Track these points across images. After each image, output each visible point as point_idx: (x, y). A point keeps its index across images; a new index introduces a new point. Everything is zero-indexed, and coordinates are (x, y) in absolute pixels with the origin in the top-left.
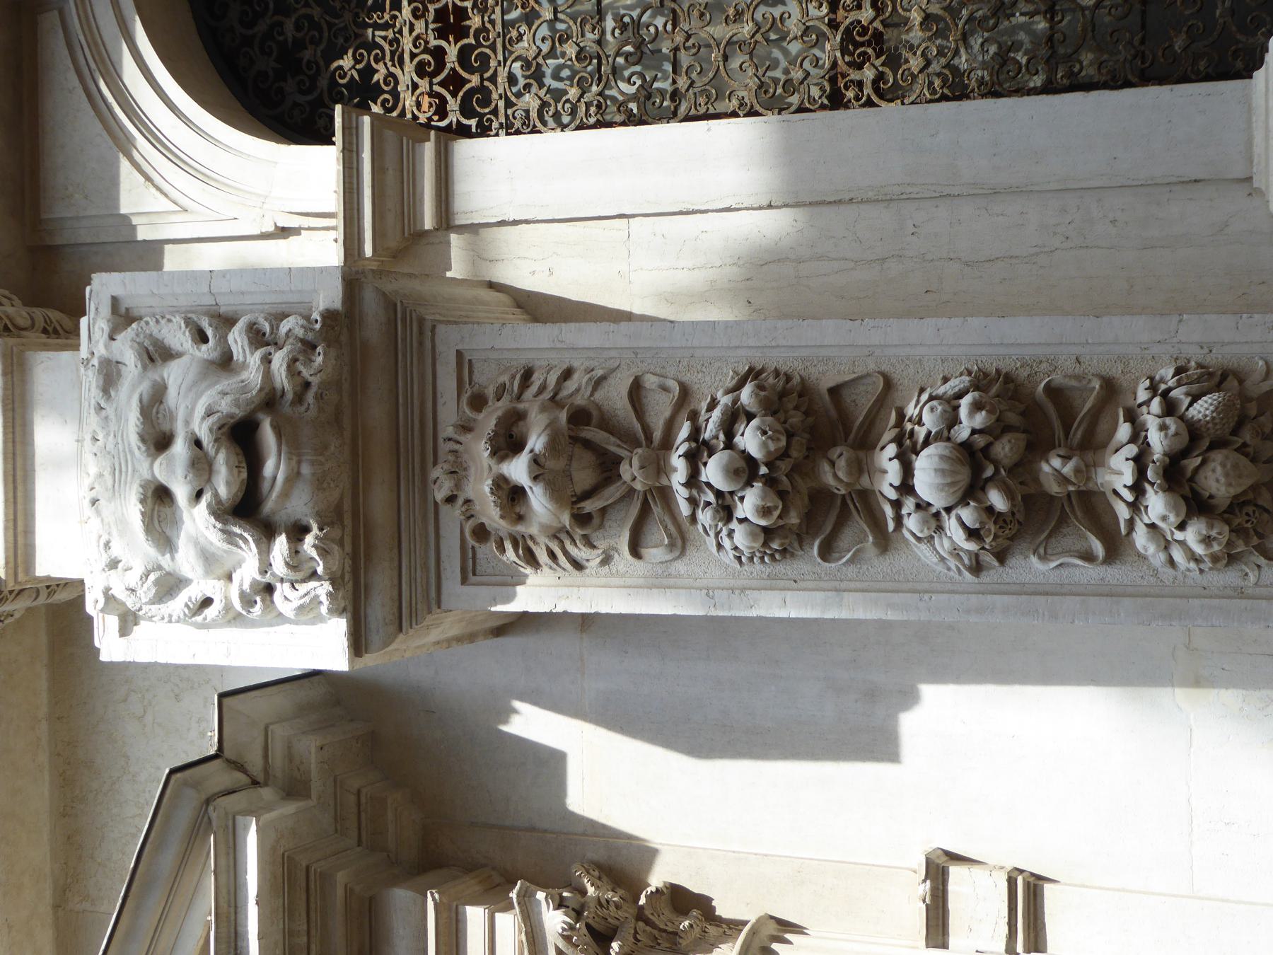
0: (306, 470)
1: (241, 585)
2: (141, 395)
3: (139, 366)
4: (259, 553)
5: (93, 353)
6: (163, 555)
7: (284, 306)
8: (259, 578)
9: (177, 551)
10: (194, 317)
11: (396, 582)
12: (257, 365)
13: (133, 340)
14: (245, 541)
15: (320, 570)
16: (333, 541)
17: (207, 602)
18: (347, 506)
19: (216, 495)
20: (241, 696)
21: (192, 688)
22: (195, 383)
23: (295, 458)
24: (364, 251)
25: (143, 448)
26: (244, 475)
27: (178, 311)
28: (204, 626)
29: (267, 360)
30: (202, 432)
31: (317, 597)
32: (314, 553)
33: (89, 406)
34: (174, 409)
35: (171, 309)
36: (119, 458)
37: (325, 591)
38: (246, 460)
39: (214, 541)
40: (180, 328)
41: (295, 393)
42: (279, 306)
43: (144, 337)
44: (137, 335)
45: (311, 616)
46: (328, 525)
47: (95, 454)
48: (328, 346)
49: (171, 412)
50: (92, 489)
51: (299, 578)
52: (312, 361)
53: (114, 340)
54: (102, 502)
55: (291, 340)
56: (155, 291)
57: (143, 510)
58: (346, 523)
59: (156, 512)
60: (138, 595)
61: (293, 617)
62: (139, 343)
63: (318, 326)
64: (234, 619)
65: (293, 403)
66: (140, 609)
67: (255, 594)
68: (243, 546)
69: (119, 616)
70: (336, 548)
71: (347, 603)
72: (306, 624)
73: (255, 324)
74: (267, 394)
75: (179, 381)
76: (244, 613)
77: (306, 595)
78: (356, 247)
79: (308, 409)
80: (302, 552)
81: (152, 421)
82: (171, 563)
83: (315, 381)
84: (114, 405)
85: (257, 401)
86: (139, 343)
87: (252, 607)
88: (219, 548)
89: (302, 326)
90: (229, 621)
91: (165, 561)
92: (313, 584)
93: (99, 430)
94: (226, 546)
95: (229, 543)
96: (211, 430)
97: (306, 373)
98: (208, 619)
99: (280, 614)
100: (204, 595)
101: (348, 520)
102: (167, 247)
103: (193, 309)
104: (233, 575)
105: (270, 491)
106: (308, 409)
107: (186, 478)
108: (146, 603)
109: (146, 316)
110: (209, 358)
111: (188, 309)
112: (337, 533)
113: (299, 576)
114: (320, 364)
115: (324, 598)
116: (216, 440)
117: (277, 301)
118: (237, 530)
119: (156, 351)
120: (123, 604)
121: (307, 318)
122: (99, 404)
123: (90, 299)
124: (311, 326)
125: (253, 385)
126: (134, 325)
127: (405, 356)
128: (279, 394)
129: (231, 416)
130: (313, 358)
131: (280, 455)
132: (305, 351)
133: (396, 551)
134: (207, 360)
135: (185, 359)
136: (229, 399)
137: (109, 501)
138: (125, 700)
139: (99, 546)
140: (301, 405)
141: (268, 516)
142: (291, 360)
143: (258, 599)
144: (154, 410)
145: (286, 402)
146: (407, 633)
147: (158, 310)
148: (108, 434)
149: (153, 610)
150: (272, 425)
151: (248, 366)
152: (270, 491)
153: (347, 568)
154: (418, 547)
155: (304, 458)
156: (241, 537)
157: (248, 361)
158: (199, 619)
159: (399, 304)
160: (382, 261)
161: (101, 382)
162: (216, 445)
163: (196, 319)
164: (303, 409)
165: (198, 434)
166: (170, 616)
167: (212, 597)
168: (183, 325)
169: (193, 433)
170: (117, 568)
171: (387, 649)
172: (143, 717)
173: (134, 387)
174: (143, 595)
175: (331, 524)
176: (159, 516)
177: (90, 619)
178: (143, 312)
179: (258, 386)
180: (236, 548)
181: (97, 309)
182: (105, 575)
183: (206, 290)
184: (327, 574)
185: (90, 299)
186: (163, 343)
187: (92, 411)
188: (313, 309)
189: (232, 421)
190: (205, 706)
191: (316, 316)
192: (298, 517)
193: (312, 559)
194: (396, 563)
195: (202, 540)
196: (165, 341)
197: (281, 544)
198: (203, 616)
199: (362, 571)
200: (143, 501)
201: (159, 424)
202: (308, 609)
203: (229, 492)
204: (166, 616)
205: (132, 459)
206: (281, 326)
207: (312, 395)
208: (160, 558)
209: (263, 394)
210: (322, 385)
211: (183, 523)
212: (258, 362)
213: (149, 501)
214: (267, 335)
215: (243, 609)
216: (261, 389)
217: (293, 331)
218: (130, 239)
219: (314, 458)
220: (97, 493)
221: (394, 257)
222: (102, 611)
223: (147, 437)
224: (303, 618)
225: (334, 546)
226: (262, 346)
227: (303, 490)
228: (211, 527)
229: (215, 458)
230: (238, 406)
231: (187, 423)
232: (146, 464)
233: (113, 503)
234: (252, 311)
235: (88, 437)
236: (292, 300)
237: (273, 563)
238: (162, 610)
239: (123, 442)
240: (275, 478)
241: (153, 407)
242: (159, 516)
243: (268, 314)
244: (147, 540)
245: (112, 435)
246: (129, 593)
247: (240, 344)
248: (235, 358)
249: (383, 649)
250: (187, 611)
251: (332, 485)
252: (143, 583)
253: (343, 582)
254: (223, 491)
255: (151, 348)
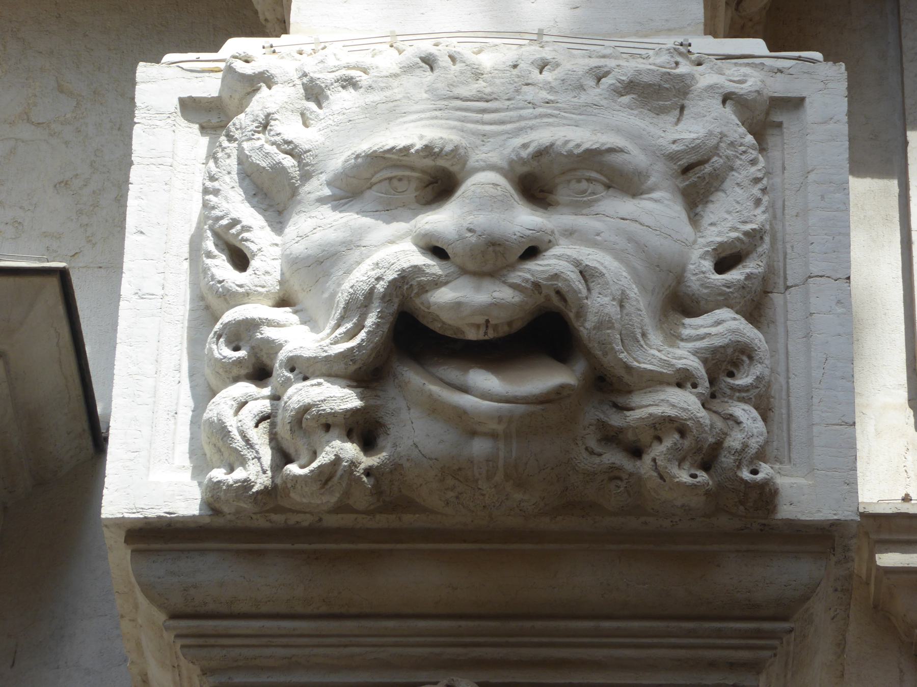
0: (480, 447)
1: (270, 323)
2: (621, 150)
3: (675, 147)
4: (328, 359)
5: (699, 64)
6: (329, 184)
7: (784, 411)
8: (282, 355)
9: (334, 208)
10: (765, 247)
11: (264, 609)
12: (674, 361)
13: (723, 136)
14: (351, 335)
15: (293, 469)
16: (347, 494)
17: (240, 260)
18: (409, 520)
19: (437, 283)
20: (61, 309)
21: (80, 212)
22: (641, 247)
23: (500, 428)
24: (887, 551)
25: (524, 154)
26: (472, 335)
27: (774, 217)
28: (196, 252)
29: (683, 380)
30: (552, 261)
31: (243, 462)
32: (324, 458)
33: (604, 57)
34: (597, 208)
35: (779, 204)
36: (508, 109)
37: (252, 478)
38: (500, 339)
39: (351, 276)
40: (745, 222)
41: (621, 430)
42: (784, 402)
43: (727, 157)
44: (732, 144)
45: (208, 450)
46: (377, 486)
47: (515, 66)
48: (708, 493)
49: (589, 204)
50: (453, 58)
51: (279, 429)
52: (681, 462)
53: (724, 102)
54: (428, 77)
55: (720, 424)
56: (812, 177)
57: (413, 151)
58: (378, 517)
59: (407, 173)
60: (257, 136)
61: (206, 416)
62: (717, 147)
63: (746, 474)
64: (207, 308)
65: (602, 426)
66: (231, 138)
67: (253, 348)
68: (342, 329)
69: (219, 98)
70: (332, 499)
71: (229, 517)
72: (193, 438)
73: (751, 358)
74: (620, 379)
75: (646, 220)
76: (218, 326)
77: (247, 441)
78: (895, 537)
79: (592, 453)
80: (327, 436)
81: (575, 169)
82: (313, 196)
83: (644, 466)
84: (604, 102)
85: (607, 361)
86: (717, 147)
87: (228, 343)
88: (339, 285)
89: (745, 446)
90: (202, 298)
91: (317, 187)
92: (267, 454)
93: (558, 73)
94: (342, 298)
95: (348, 304)
96: (556, 276)
97: (659, 450)
98: (208, 261)
99: (214, 394)
100: (254, 255)
101: (383, 521)
102: (893, 185)
103: (780, 245)
104: (288, 309)
105: (442, 380)
106: (592, 453)
107: (470, 230)
108: (240, 150)
109: (767, 160)
110: (688, 275)
111: (779, 236)
112: (361, 501)
113: (283, 430)
114: (675, 477)
115: (239, 474)
116: (537, 286)
117: (792, 400)
118: (371, 320)
119: (702, 178)
120: (241, 109)
121: (761, 455)
122: (606, 74)
123: (799, 59)
124: (745, 462)
125: (638, 354)
126: (750, 139)
127: (689, 634)
128: (621, 400)
129: (581, 313)
130: (686, 465)
131: (507, 401)
132: (700, 449)
133: (324, 609)
134: (684, 270)
135: (687, 230)
136: (612, 309)
137: (431, 90)
138: (61, 89)
139: (348, 67)
140: (599, 441)
141: (395, 376)
142: (684, 425)
143: (242, 353)
144: (594, 175)
145: (603, 412)
146: (167, 628)
147: (777, 180)
148: (551, 90)
149: (228, 161)
150: (562, 387)
151: (672, 345)
152: (442, 380)
153: (293, 519)
154: (329, 651)
155: (501, 445)
156: (359, 327)
157: (682, 344)
158: (209, 244)
159: (786, 625)
160: (868, 584)
161: (646, 79)
162: (529, 286)
163: (760, 250)
164: (592, 443)
165: (549, 253)
166: (216, 192)
167: (250, 271)
168: (748, 227)
169: (550, 244)
170: (308, 99)
171: (137, 590)
172: (29, 120)
173: (635, 137)
174: (258, 144)
175: (378, 491)
176: (400, 180)
177: (215, 47)
178: (775, 154)
179: (636, 364)
180: (337, 315)
181: (780, 71)
182: (295, 76)
183: (815, 270)
184: (285, 482)
185: (799, 59)
186: (717, 190)
187: (595, 62)
188: (777, 466)
189: (572, 315)
190: (45, 235)
191: (765, 471)
192: (393, 431)
193: (314, 455)
194: (299, 609)
195: (355, 254)
196: (721, 194)
197: (343, 399)
198: (215, 251)
199: (288, 546)
200: (428, 150)
201: (569, 181)
202: (220, 444)
203: (441, 307)
204: (216, 184)
205: (507, 132)
206: (747, 407)
207: (618, 462)
208: (323, 177)
209: (622, 372)
210: (635, 483)
211: (388, 222)
212: (680, 364)
213: (429, 162)
214: (730, 380)
215: (226, 325)
216: (628, 368)
217: (736, 429)
218: (910, 118)
219: (501, 463)
220: (445, 68)
221: (875, 607)
222: (230, 70)
223: (545, 160)
224: (203, 437)
225: (338, 495)
226: (708, 372)
227: (442, 441)
228: (377, 272)
229: (504, 282)
230: (599, 326)
231: (570, 233)
232: (495, 158)
233: (425, 96)
234: (774, 352)
235: (547, 53)
236: (794, 426)
237: (308, 383)
238: (227, 178)
239: (536, 117)
240: (465, 390)
241: (600, 172)
242: (400, 180)
243: (769, 382)
244: (358, 157)
245: (551, 97)
246: (261, 117)
247: (713, 330)
248: (687, 321)
249: (139, 583)
250: (224, 222)
251: (450, 495)
252: (278, 146)
253: (267, 511)
254: (444, 296)
255: (708, 168)
